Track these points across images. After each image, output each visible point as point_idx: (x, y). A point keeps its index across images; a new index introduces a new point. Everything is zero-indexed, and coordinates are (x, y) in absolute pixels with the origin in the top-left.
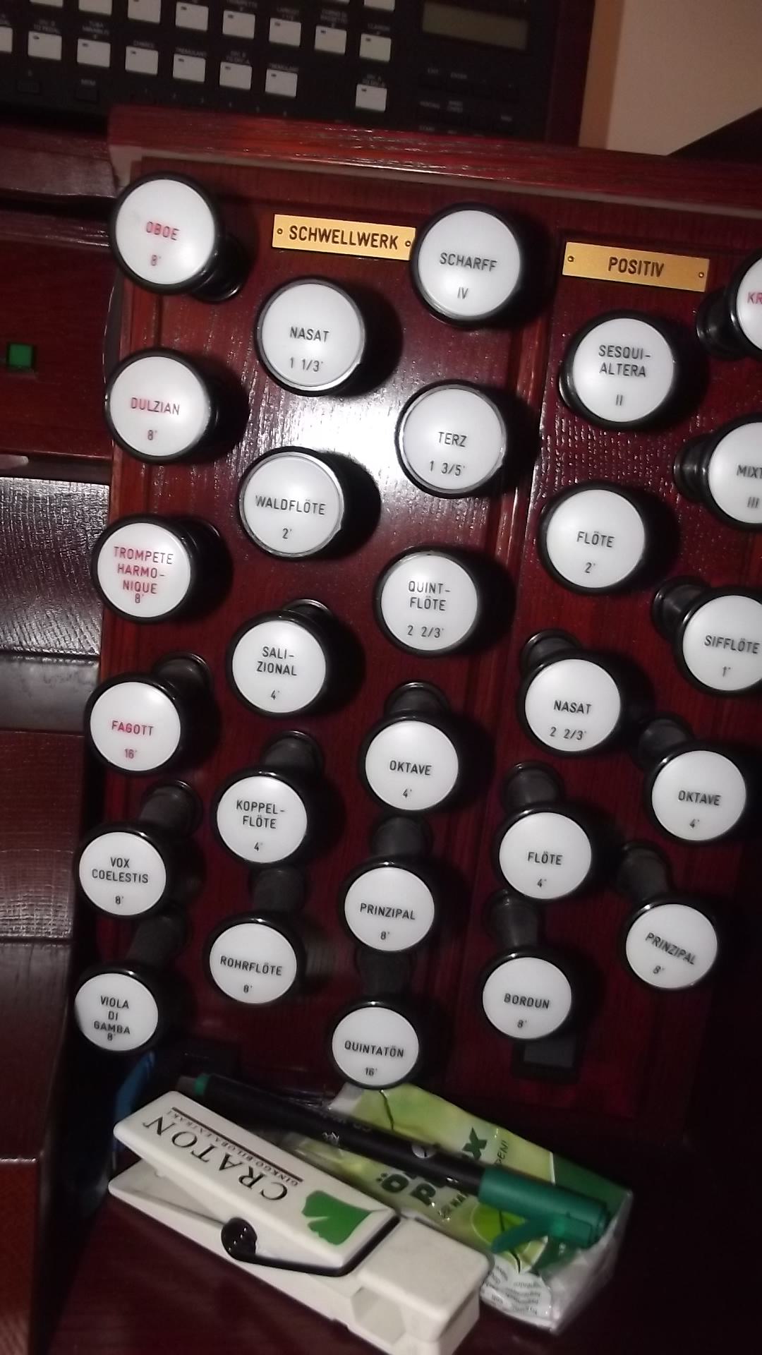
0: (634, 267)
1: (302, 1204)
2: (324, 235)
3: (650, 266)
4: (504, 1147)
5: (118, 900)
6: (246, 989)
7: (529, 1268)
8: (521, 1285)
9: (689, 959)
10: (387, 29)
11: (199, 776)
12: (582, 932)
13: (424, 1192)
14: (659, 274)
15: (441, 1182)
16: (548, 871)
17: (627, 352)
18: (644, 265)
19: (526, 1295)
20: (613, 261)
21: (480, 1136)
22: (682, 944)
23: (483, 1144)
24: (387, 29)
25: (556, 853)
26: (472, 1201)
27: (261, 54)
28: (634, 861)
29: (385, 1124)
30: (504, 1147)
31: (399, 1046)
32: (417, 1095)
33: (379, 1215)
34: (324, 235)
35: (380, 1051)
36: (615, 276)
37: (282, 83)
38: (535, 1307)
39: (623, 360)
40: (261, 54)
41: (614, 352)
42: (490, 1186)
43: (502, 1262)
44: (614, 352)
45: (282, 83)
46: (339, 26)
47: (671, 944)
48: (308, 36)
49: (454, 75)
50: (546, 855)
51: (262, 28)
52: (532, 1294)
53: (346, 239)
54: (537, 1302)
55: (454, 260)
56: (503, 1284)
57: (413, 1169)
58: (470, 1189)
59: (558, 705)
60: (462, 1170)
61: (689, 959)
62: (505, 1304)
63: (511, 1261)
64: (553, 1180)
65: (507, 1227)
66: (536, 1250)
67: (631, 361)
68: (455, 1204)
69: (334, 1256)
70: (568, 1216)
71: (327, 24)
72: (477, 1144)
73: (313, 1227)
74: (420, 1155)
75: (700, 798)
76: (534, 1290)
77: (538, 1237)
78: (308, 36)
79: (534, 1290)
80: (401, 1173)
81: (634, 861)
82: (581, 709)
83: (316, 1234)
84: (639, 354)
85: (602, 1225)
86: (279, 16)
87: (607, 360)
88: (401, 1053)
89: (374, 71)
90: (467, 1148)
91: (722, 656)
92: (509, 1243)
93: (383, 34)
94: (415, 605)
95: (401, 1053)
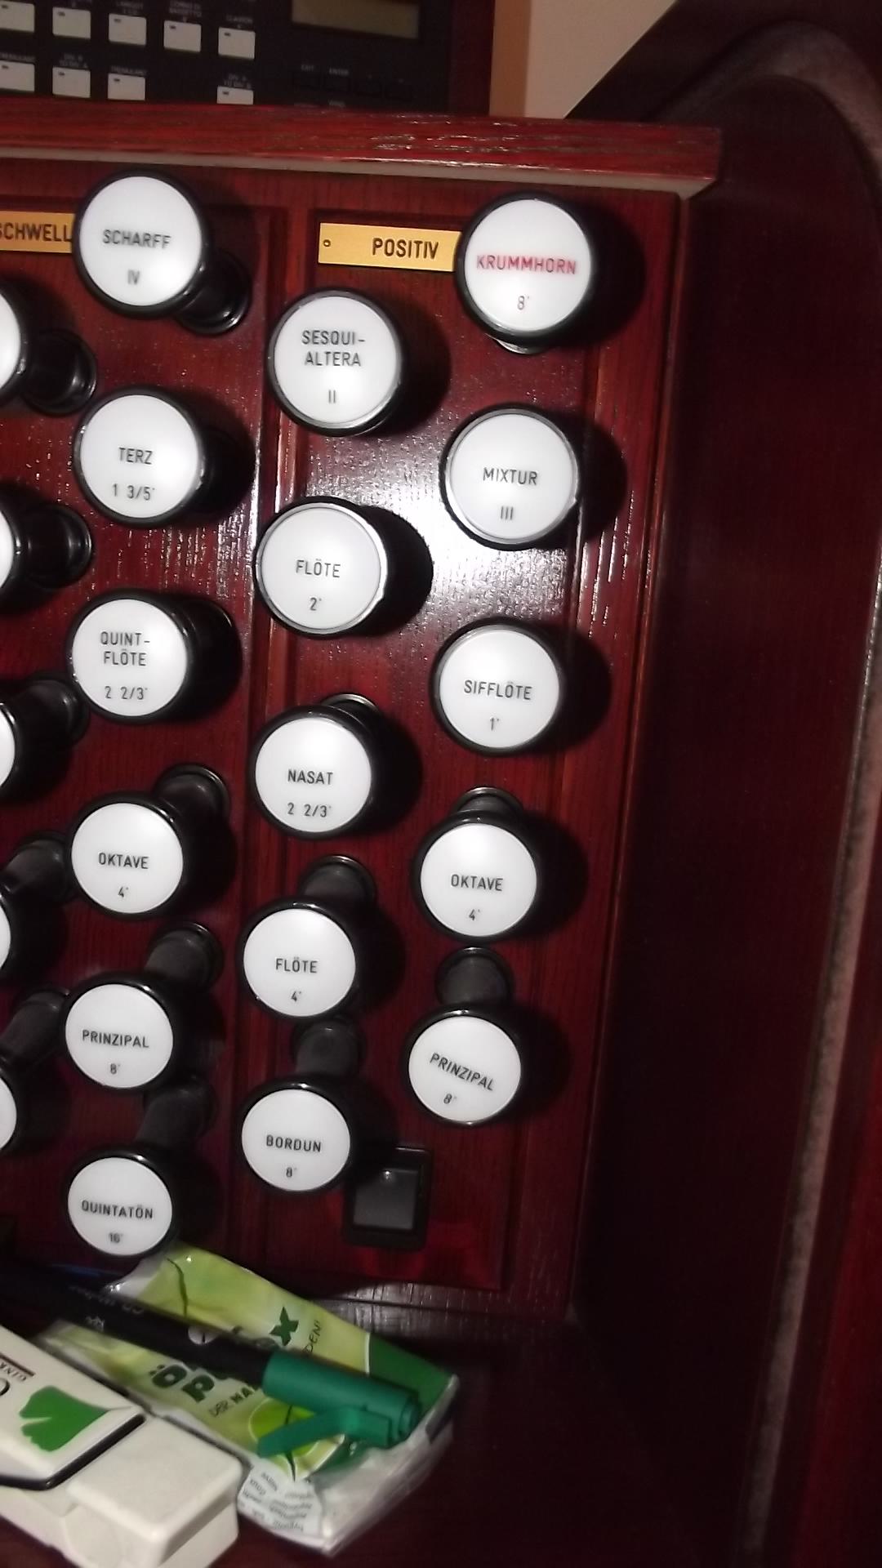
0: (402, 249)
1: (23, 1402)
2: (34, 232)
3: (422, 246)
4: (317, 1329)
5: (113, 1069)
6: (289, 1172)
7: (306, 1474)
8: (293, 1495)
9: (485, 1083)
10: (250, 21)
11: (219, 918)
12: (359, 1057)
13: (199, 1386)
14: (433, 254)
15: (222, 1372)
16: (301, 981)
17: (335, 337)
18: (414, 246)
19: (295, 1507)
20: (377, 244)
21: (291, 1317)
22: (474, 1067)
23: (294, 1326)
24: (250, 21)
25: (310, 958)
26: (258, 1397)
27: (100, 55)
28: (408, 967)
29: (177, 1309)
30: (317, 1329)
31: (146, 1205)
32: (197, 1262)
33: (121, 1411)
34: (34, 232)
35: (123, 1212)
36: (381, 260)
37: (127, 87)
38: (300, 1522)
39: (331, 348)
40: (100, 55)
41: (320, 339)
42: (274, 1373)
43: (262, 1467)
44: (320, 339)
45: (127, 87)
46: (191, 20)
47: (465, 1066)
48: (155, 33)
49: (334, 71)
50: (296, 961)
51: (100, 26)
52: (303, 1506)
53: (60, 235)
54: (304, 1516)
55: (119, 238)
56: (270, 1495)
57: (192, 1356)
58: (254, 1379)
59: (292, 776)
60: (238, 1357)
61: (485, 1083)
62: (268, 1520)
63: (281, 1465)
64: (367, 1370)
65: (291, 1420)
66: (322, 1452)
67: (340, 348)
68: (236, 1398)
69: (43, 1465)
70: (364, 1409)
71: (177, 18)
72: (287, 1326)
73: (28, 1431)
74: (196, 1339)
75: (478, 881)
76: (307, 1501)
77: (329, 1434)
78: (155, 33)
79: (307, 1501)
80: (182, 1365)
81: (408, 967)
82: (321, 779)
83: (29, 1439)
84: (350, 338)
85: (407, 1418)
86: (120, 11)
87: (312, 348)
88: (149, 1214)
89: (235, 69)
90: (275, 1332)
91: (487, 704)
92: (283, 1443)
93: (246, 27)
94: (110, 661)
95: (149, 1214)
